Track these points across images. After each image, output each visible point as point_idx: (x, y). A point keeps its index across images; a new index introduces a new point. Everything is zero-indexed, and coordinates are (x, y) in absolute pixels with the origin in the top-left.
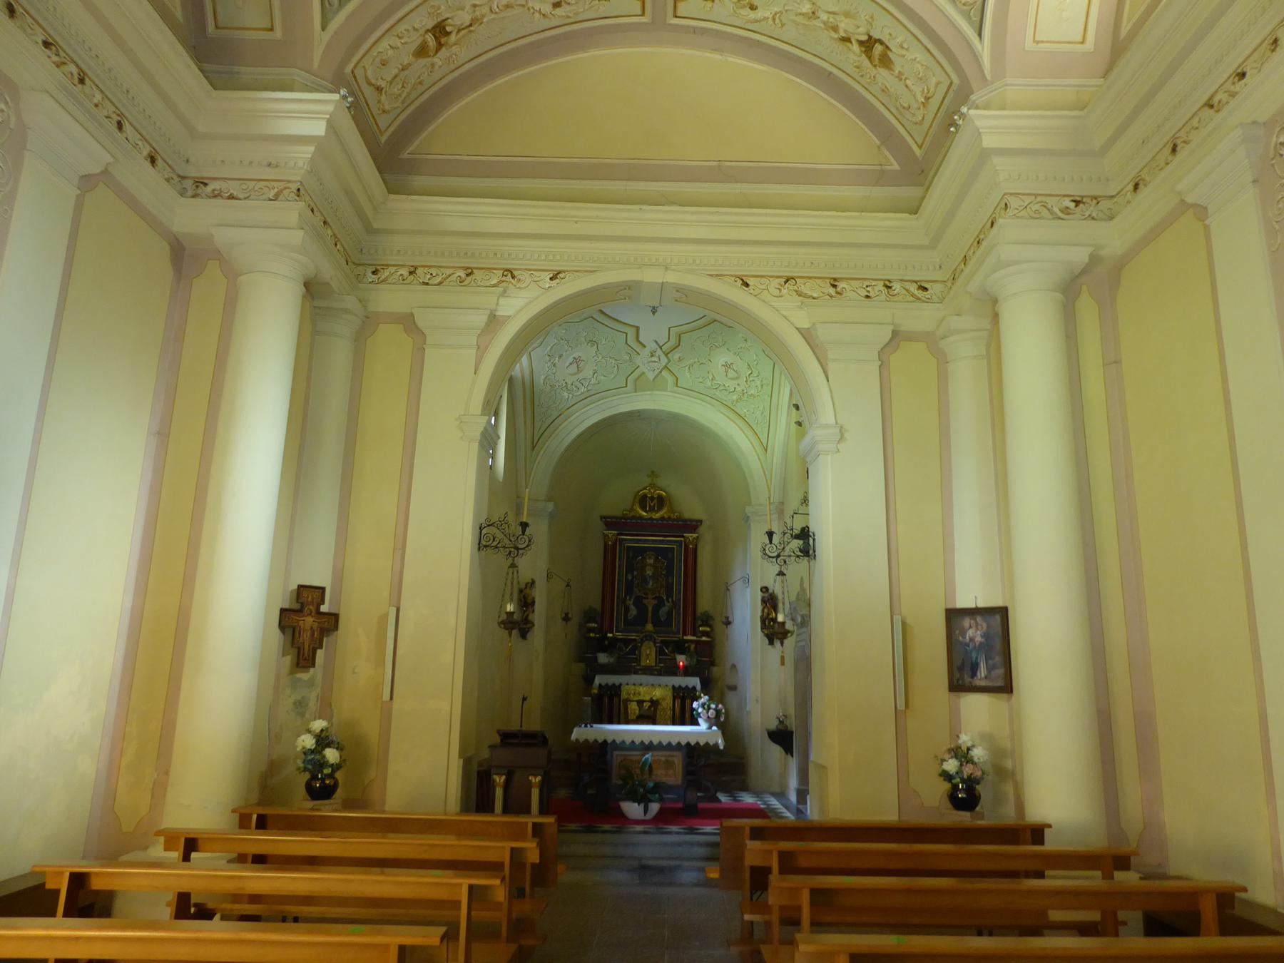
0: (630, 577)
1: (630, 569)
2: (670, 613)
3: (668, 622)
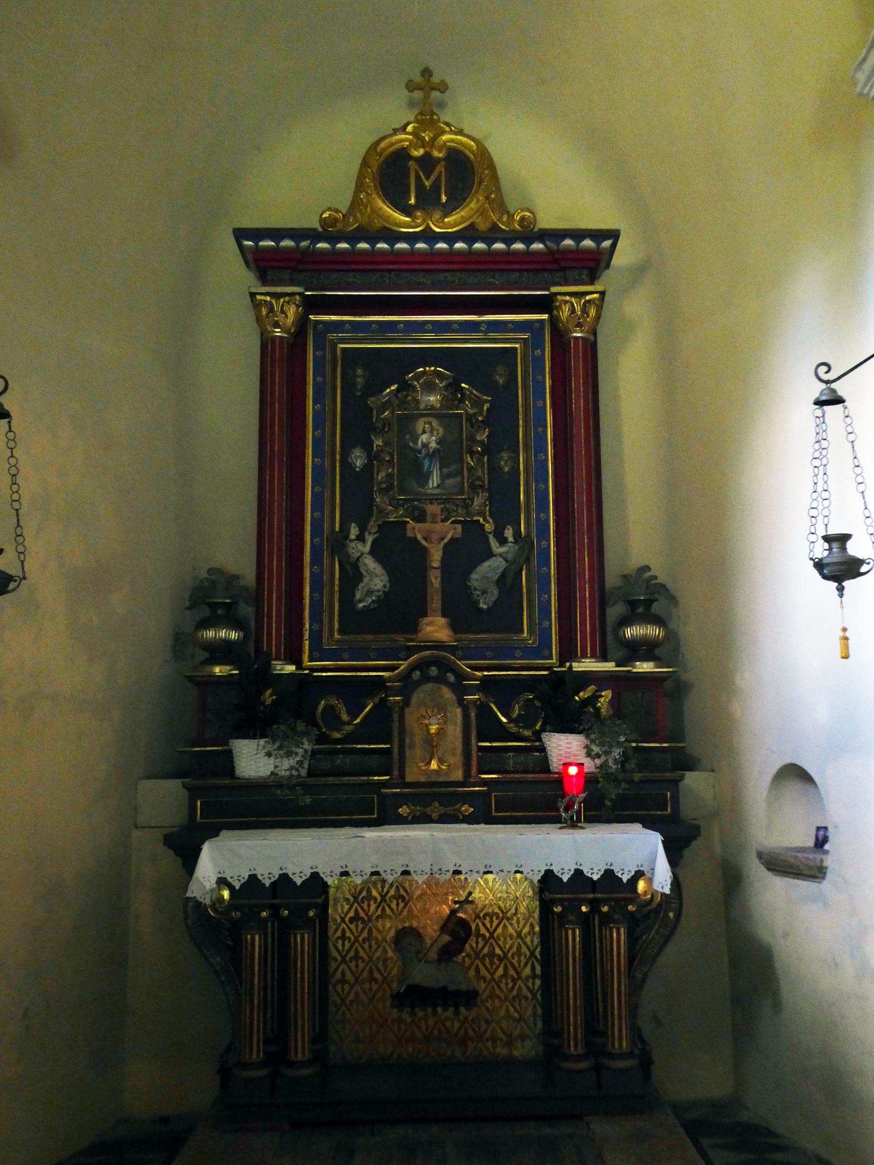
0: (358, 459)
1: (359, 427)
2: (508, 583)
3: (505, 615)
